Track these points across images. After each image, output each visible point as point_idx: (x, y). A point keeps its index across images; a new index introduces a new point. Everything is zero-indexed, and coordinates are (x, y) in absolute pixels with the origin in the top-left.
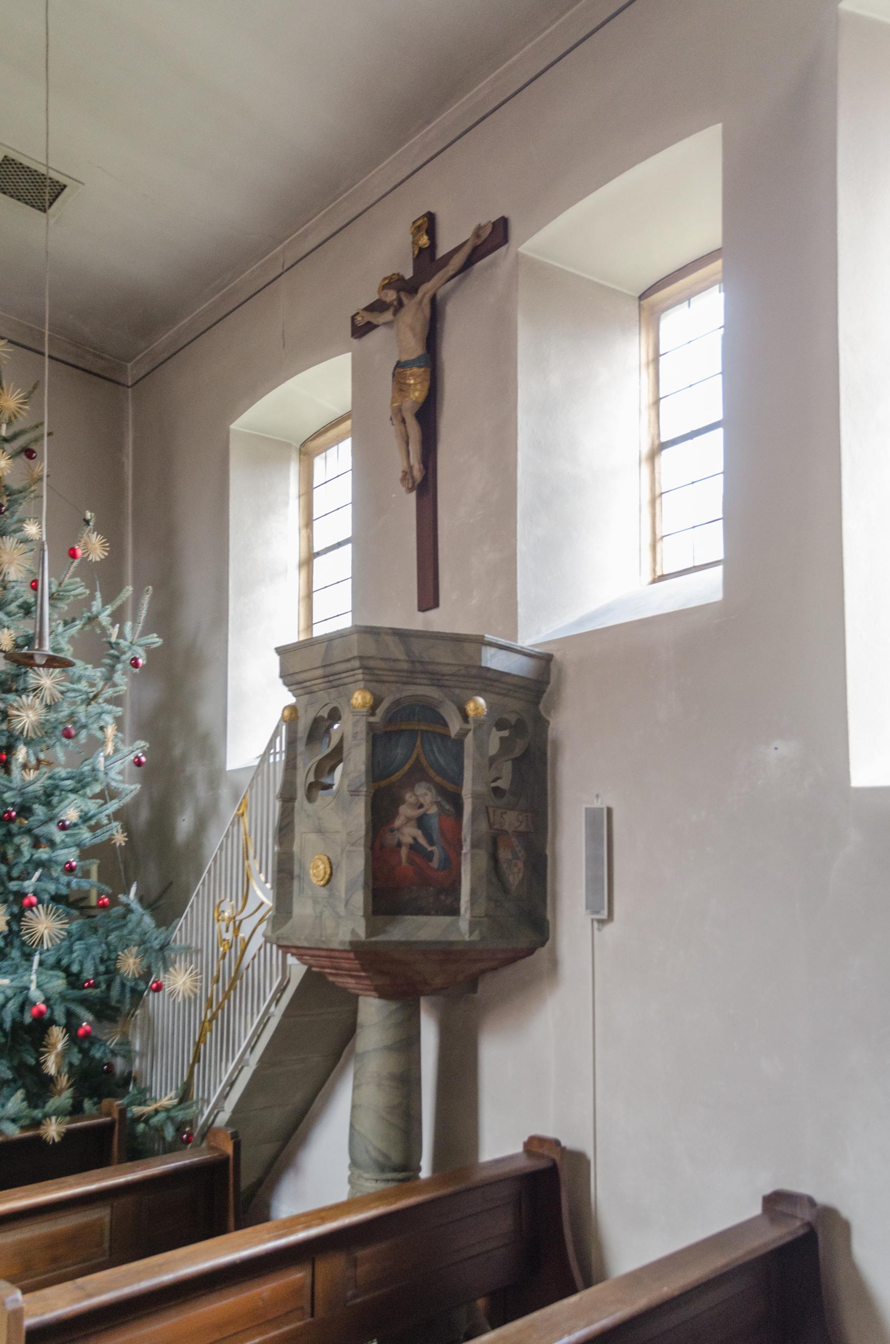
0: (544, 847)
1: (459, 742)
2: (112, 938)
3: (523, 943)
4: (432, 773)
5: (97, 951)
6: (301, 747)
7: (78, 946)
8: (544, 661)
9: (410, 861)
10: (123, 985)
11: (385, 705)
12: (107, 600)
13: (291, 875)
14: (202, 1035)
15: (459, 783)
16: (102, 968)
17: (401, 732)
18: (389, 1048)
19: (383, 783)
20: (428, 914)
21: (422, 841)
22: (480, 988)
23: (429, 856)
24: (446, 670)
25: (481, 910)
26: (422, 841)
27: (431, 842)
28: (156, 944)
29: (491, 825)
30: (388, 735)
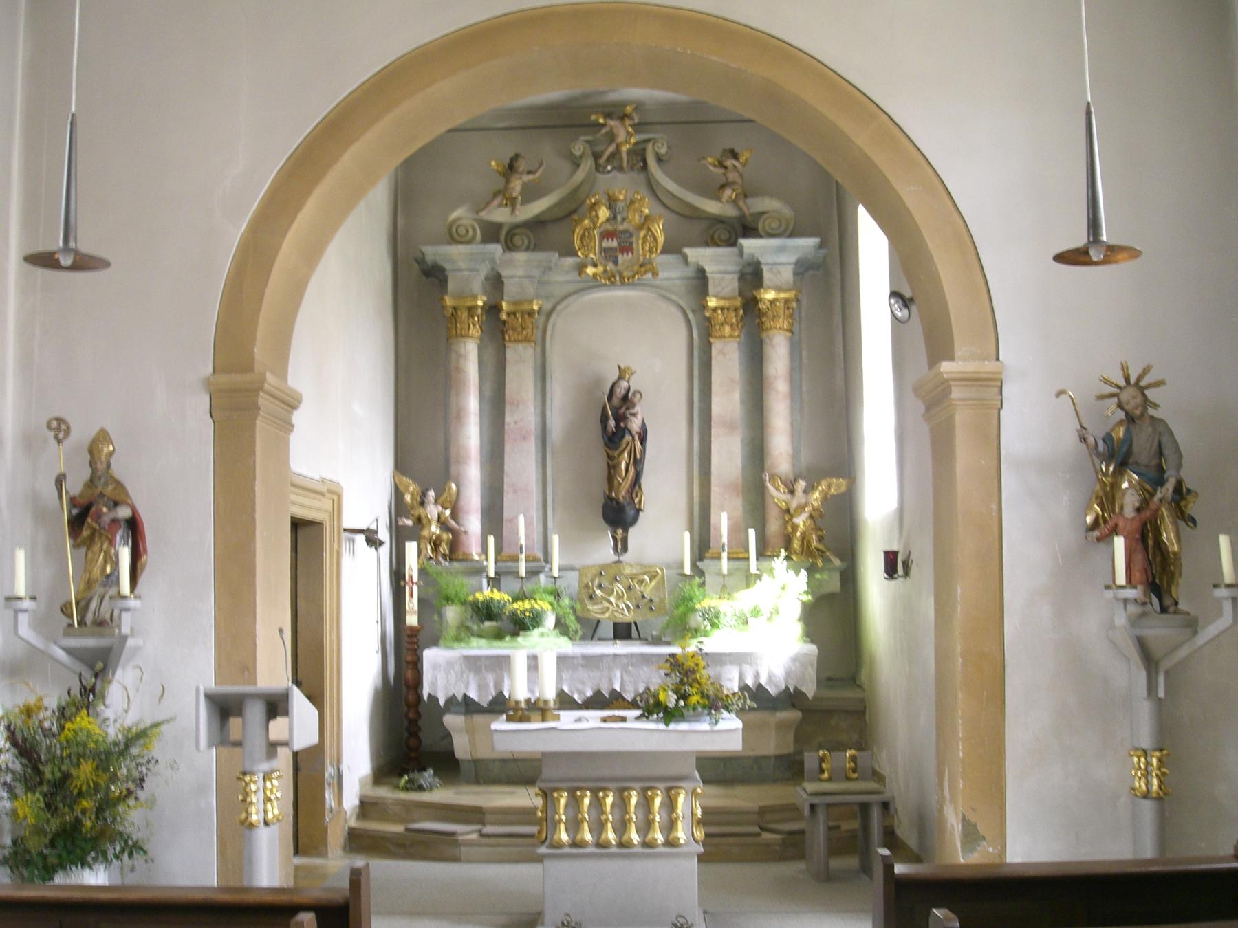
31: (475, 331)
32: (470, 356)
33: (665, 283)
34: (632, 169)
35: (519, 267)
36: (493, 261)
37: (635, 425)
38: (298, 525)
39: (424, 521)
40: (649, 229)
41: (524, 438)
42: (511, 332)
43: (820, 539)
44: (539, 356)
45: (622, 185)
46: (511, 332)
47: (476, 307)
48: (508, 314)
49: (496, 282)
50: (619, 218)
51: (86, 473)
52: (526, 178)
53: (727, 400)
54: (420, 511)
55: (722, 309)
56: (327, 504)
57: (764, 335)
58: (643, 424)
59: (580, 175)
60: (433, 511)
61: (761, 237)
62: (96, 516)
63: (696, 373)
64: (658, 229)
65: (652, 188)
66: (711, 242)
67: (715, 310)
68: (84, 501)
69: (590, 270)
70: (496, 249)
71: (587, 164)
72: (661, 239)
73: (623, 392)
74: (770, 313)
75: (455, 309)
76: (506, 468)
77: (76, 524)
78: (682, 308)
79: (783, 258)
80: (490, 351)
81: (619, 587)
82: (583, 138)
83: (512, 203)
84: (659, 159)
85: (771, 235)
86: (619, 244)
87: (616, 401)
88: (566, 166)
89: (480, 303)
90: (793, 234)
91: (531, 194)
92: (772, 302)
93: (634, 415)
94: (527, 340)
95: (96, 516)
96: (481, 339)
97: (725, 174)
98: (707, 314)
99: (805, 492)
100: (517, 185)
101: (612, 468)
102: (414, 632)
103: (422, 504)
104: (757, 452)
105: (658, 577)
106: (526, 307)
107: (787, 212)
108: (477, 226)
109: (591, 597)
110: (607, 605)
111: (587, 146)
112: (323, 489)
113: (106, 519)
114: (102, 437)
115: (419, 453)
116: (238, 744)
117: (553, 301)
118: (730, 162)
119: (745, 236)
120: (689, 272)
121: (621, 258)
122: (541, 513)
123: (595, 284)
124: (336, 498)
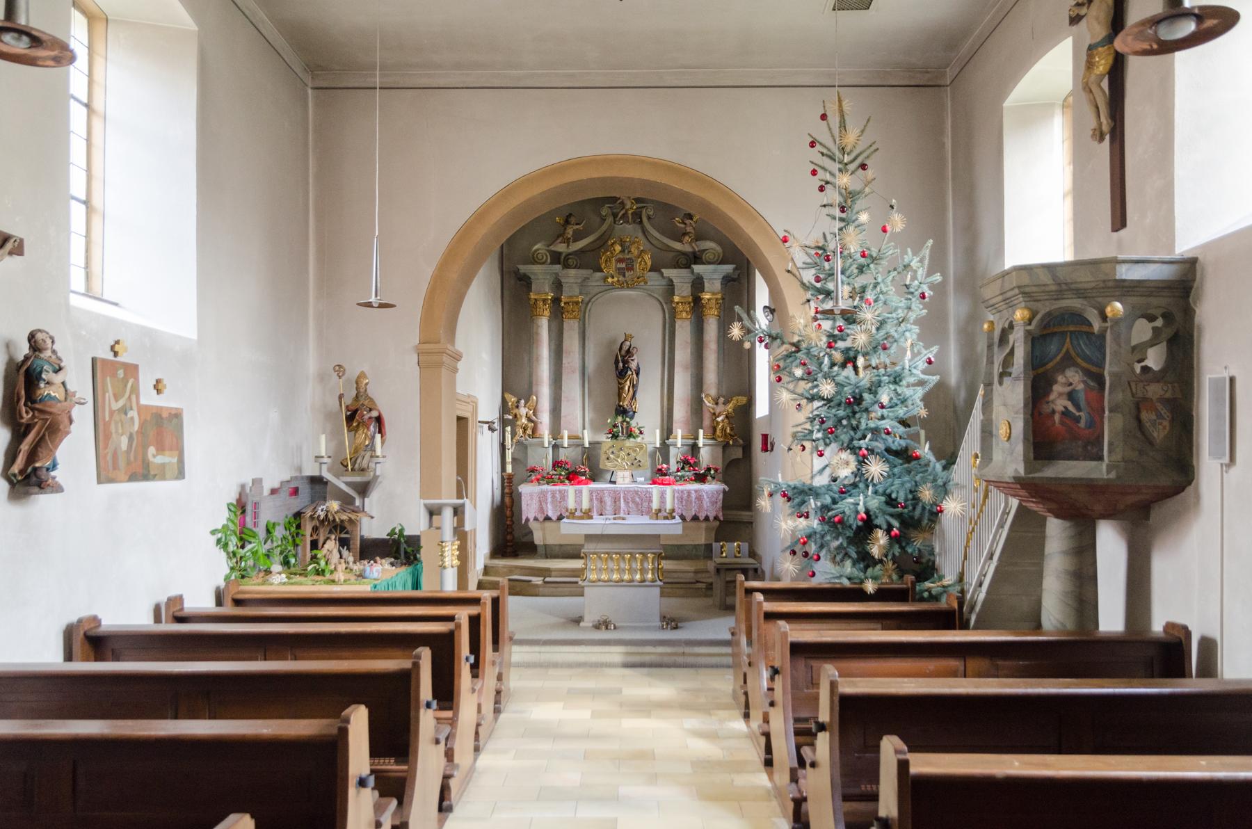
0: (1191, 410)
1: (1102, 336)
2: (918, 478)
3: (1165, 481)
4: (1079, 360)
5: (908, 485)
6: (996, 348)
7: (897, 482)
8: (1190, 265)
9: (1062, 423)
10: (924, 508)
11: (1039, 317)
12: (915, 253)
13: (991, 434)
14: (968, 542)
15: (1101, 365)
16: (910, 496)
17: (1055, 333)
18: (1065, 553)
19: (1041, 370)
20: (1077, 459)
21: (1071, 408)
22: (1153, 515)
23: (1078, 419)
24: (1086, 286)
25: (1118, 456)
26: (1071, 408)
27: (1079, 408)
28: (940, 482)
29: (1133, 395)
30: (1044, 337)
31: (547, 313)
32: (543, 326)
35: (572, 277)
37: (633, 365)
38: (459, 419)
49: (558, 285)
51: (354, 393)
53: (683, 354)
54: (516, 411)
56: (470, 408)
59: (605, 227)
60: (523, 411)
61: (703, 264)
62: (359, 415)
64: (647, 258)
65: (644, 231)
66: (677, 266)
68: (353, 408)
69: (610, 280)
70: (558, 267)
71: (610, 220)
72: (649, 263)
77: (350, 419)
81: (622, 454)
83: (567, 241)
84: (649, 218)
85: (710, 263)
90: (722, 262)
91: (578, 237)
94: (575, 318)
95: (359, 415)
100: (570, 232)
101: (621, 389)
102: (510, 478)
107: (719, 249)
113: (366, 417)
114: (362, 375)
115: (515, 382)
116: (438, 528)
118: (688, 222)
119: (695, 263)
120: (664, 282)
123: (613, 287)
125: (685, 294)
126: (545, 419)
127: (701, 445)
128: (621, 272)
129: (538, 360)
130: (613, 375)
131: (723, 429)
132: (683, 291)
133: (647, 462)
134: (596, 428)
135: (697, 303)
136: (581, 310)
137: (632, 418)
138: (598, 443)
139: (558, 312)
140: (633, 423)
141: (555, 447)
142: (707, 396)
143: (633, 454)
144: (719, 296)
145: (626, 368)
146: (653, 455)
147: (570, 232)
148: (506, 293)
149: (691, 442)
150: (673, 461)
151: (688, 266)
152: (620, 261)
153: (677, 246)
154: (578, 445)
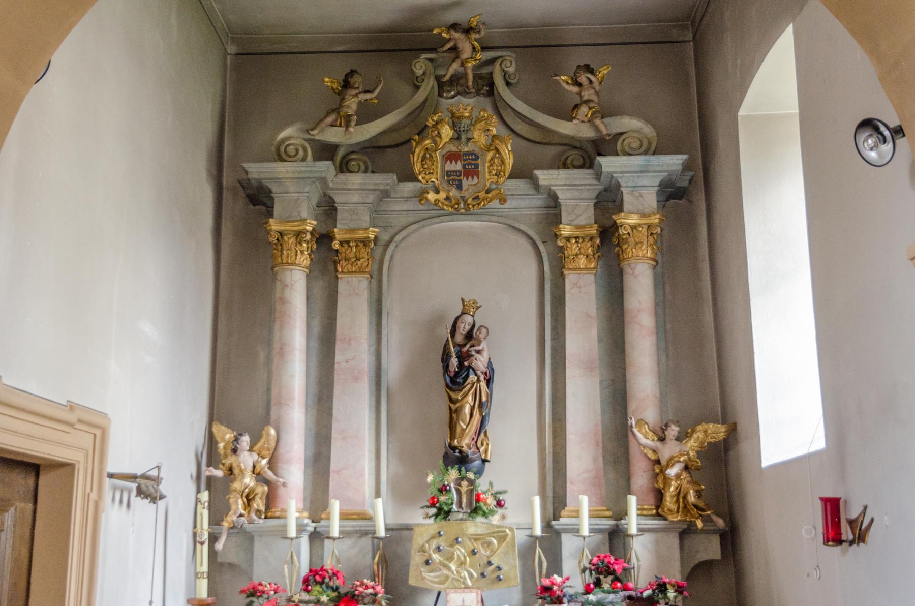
31: (304, 260)
32: (295, 285)
33: (514, 212)
34: (478, 93)
35: (356, 190)
36: (323, 180)
37: (480, 363)
39: (236, 471)
40: (498, 151)
41: (356, 379)
42: (343, 263)
43: (699, 494)
44: (374, 290)
45: (467, 105)
46: (343, 263)
47: (304, 232)
48: (341, 243)
50: (463, 137)
52: (363, 97)
53: (582, 339)
54: (231, 460)
55: (576, 238)
57: (624, 265)
58: (490, 363)
60: (246, 459)
61: (617, 154)
63: (547, 286)
64: (507, 152)
67: (568, 239)
69: (431, 196)
70: (326, 168)
72: (510, 161)
73: (468, 328)
74: (631, 240)
75: (281, 234)
76: (335, 412)
78: (530, 238)
79: (646, 181)
80: (319, 286)
81: (460, 551)
82: (424, 56)
86: (464, 166)
87: (459, 338)
88: (408, 89)
89: (309, 228)
90: (657, 151)
91: (367, 114)
92: (634, 227)
93: (478, 352)
94: (361, 271)
96: (310, 269)
97: (579, 94)
98: (560, 244)
99: (678, 439)
100: (352, 104)
103: (235, 451)
104: (617, 396)
105: (508, 539)
106: (361, 235)
108: (307, 146)
109: (427, 563)
110: (445, 572)
111: (429, 64)
112: (72, 417)
115: (235, 399)
117: (392, 231)
121: (466, 183)
122: (373, 464)
123: (438, 212)
124: (98, 432)
125: (582, 221)
126: (294, 477)
127: (633, 530)
128: (454, 180)
129: (282, 353)
130: (439, 381)
131: (680, 495)
132: (578, 216)
133: (512, 568)
134: (402, 495)
135: (608, 237)
136: (374, 255)
137: (479, 473)
138: (409, 528)
139: (327, 252)
140: (482, 485)
141: (316, 537)
142: (640, 422)
143: (483, 552)
144: (655, 219)
145: (465, 369)
146: (527, 553)
147: (352, 104)
148: (226, 227)
149: (608, 523)
150: (570, 566)
151: (588, 163)
152: (451, 157)
153: (565, 128)
154: (363, 534)
